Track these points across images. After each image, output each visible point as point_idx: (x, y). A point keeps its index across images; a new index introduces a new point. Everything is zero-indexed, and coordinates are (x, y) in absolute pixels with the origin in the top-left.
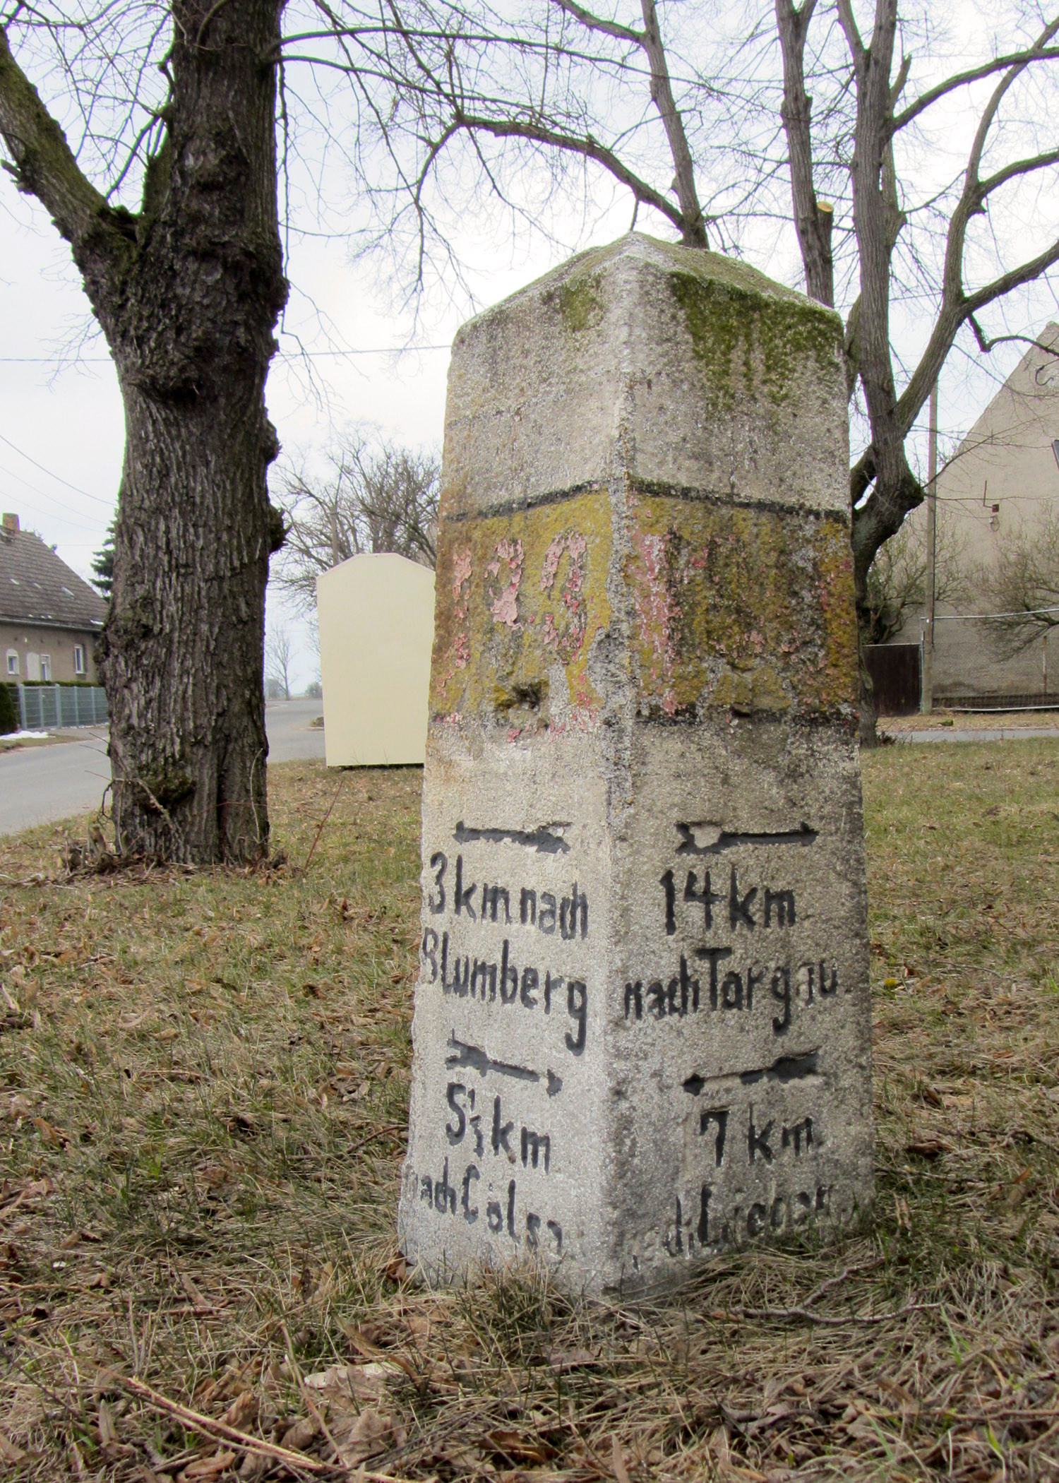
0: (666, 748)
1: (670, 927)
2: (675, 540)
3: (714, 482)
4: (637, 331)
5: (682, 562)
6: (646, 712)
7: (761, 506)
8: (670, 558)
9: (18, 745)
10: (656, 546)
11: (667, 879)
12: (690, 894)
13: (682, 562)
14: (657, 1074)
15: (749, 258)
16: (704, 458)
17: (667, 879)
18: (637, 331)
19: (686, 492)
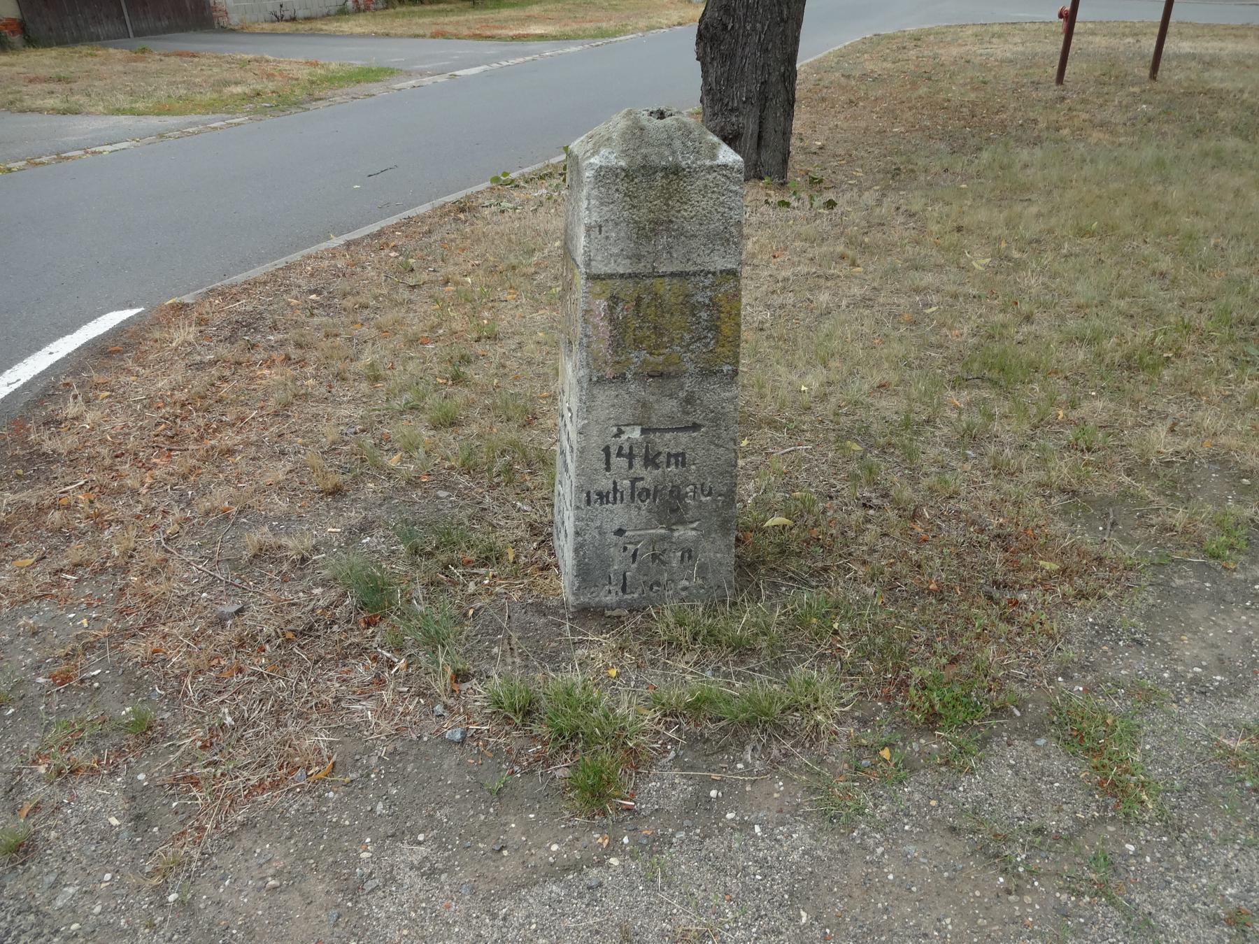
0: (605, 396)
1: (608, 469)
2: (614, 300)
3: (640, 268)
4: (593, 202)
5: (619, 309)
6: (595, 379)
7: (673, 275)
8: (611, 309)
9: (344, 36)
10: (601, 304)
11: (607, 450)
12: (619, 455)
13: (619, 309)
14: (600, 528)
15: (698, 107)
16: (639, 258)
17: (607, 450)
18: (593, 202)
19: (622, 276)
